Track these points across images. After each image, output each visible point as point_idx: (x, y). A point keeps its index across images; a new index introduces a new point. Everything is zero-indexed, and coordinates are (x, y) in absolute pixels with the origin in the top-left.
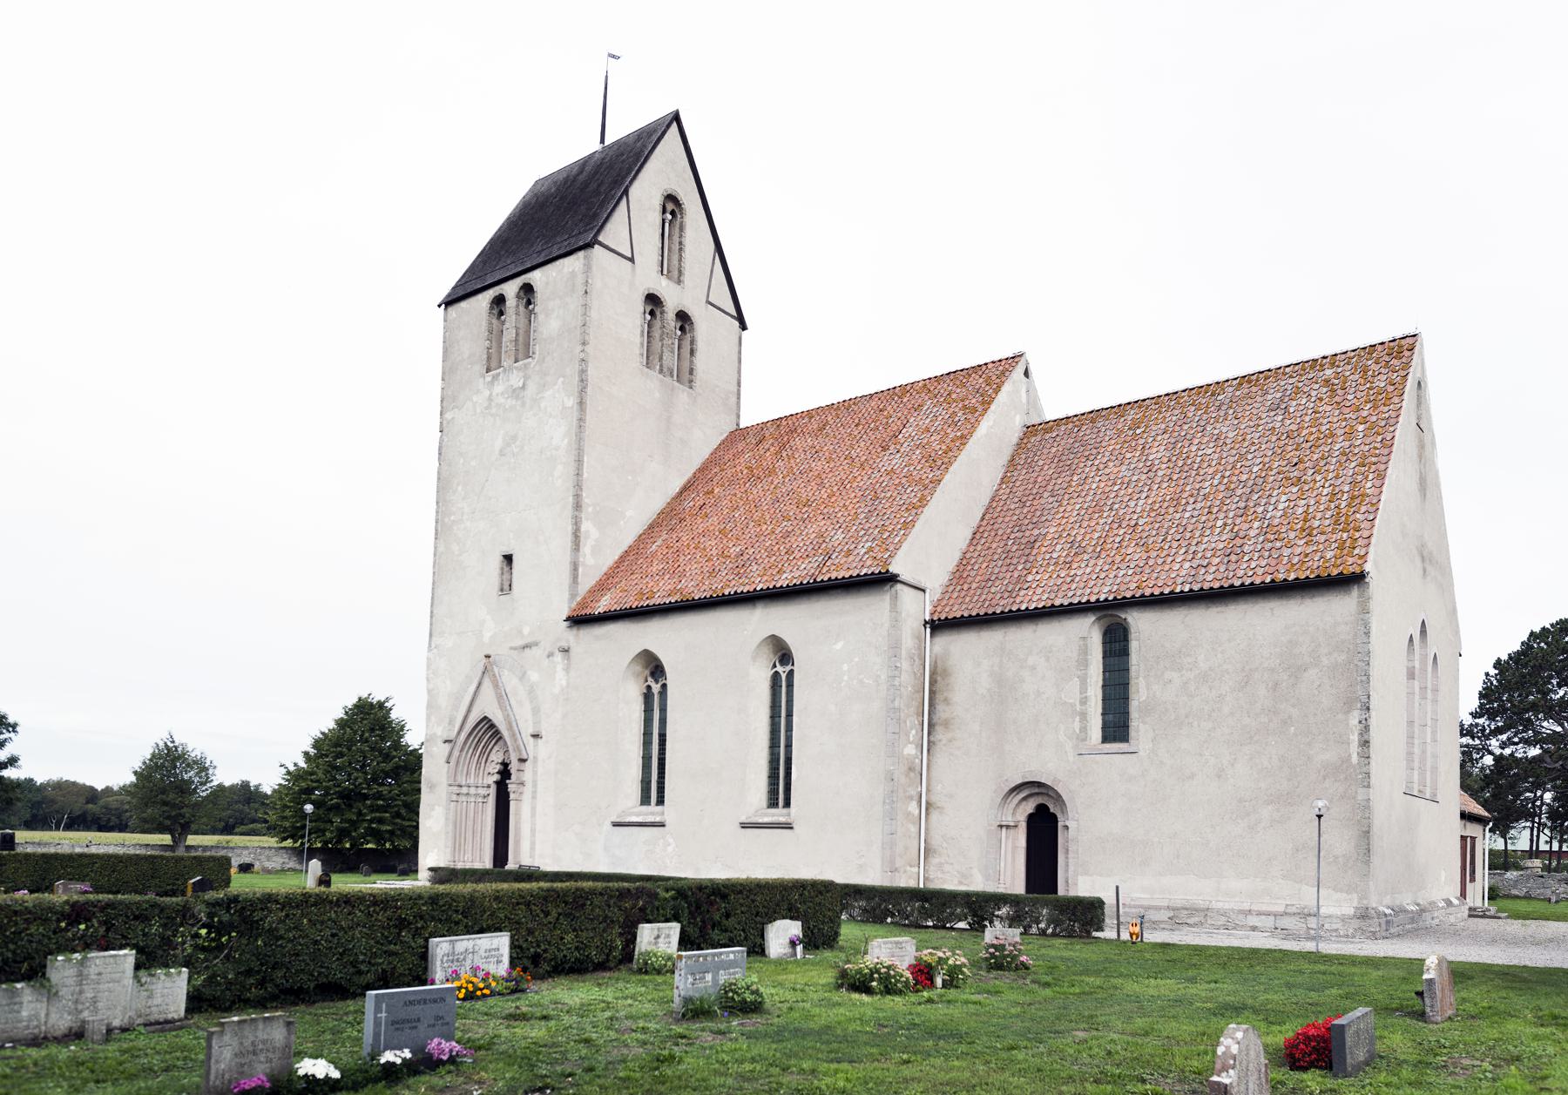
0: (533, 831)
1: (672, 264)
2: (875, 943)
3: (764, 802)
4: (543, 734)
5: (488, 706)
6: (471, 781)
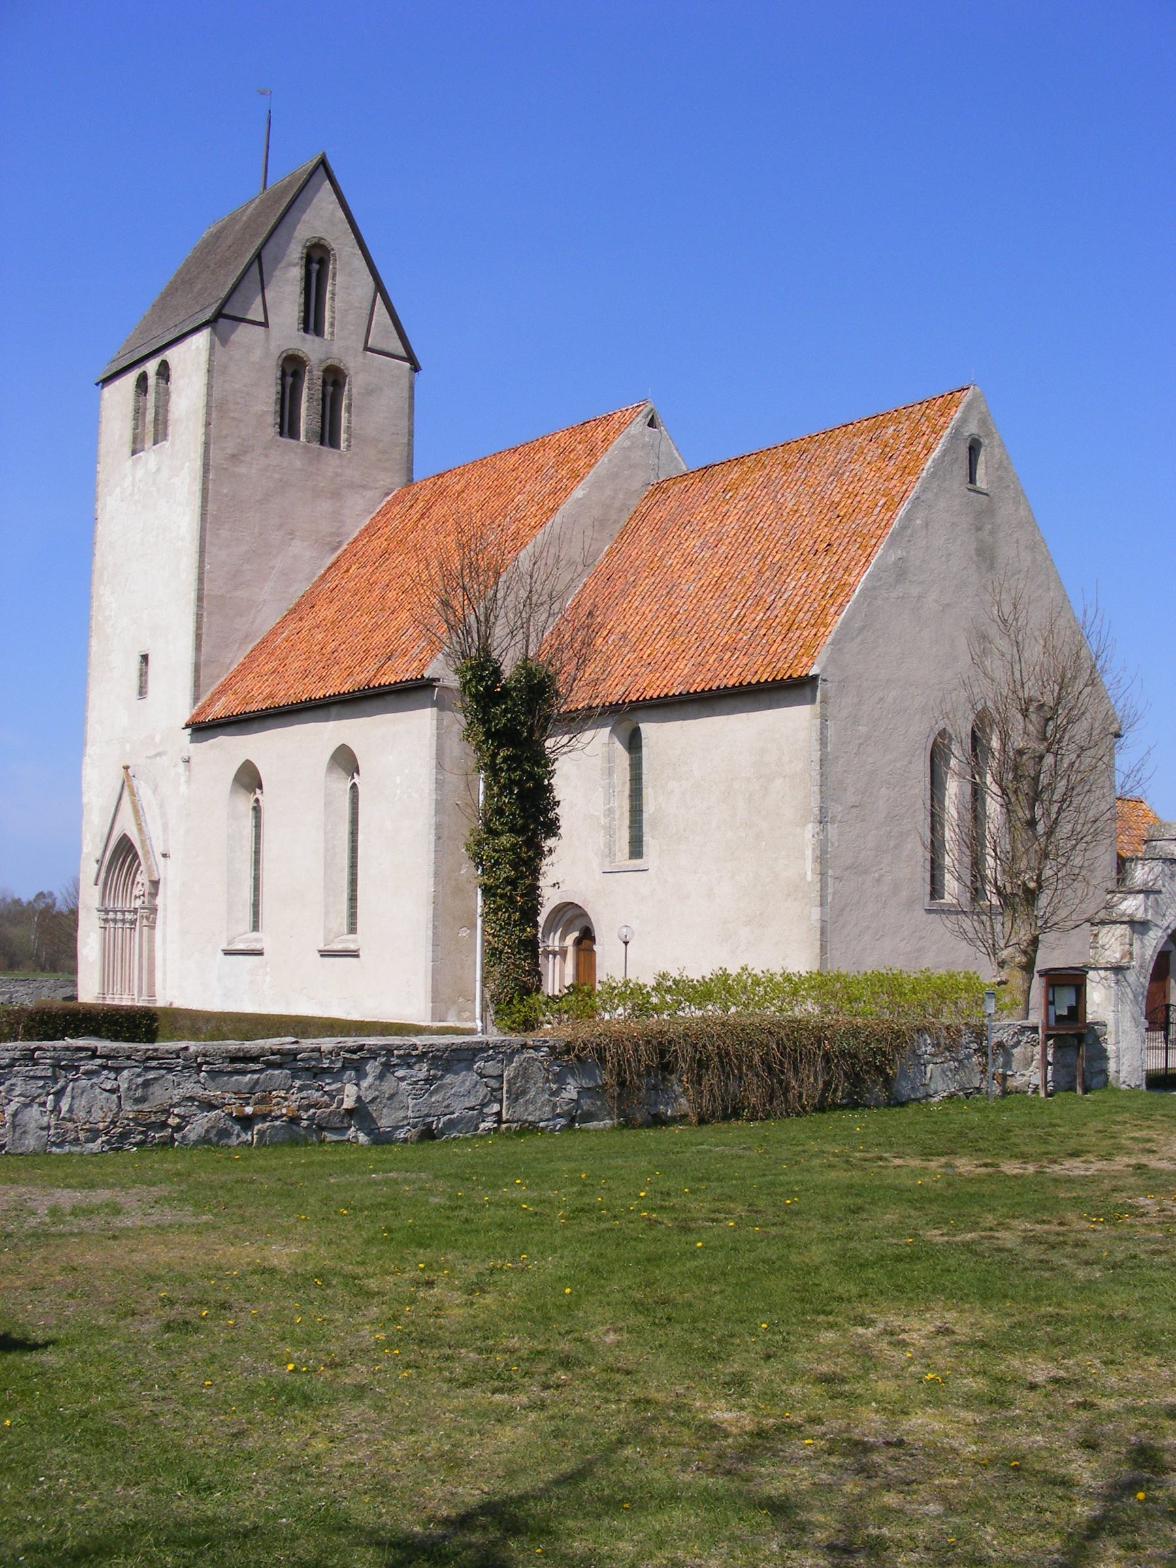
0: (164, 959)
1: (312, 321)
4: (171, 852)
5: (127, 825)
6: (119, 906)
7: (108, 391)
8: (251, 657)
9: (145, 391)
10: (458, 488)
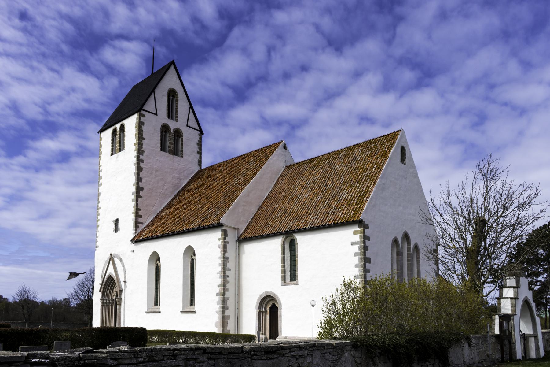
1: (171, 113)
2: (530, 357)
3: (154, 304)
5: (111, 271)
7: (104, 134)
8: (154, 219)
9: (116, 135)
10: (219, 169)
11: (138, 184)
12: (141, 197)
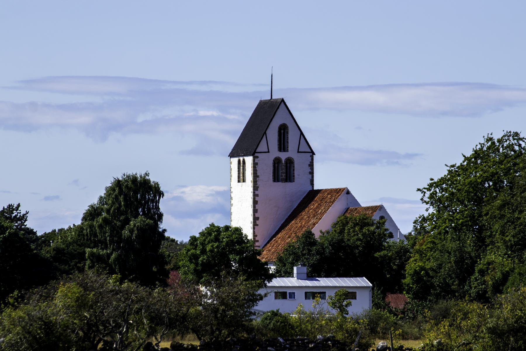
1: (283, 146)
11: (254, 215)
12: (257, 225)
